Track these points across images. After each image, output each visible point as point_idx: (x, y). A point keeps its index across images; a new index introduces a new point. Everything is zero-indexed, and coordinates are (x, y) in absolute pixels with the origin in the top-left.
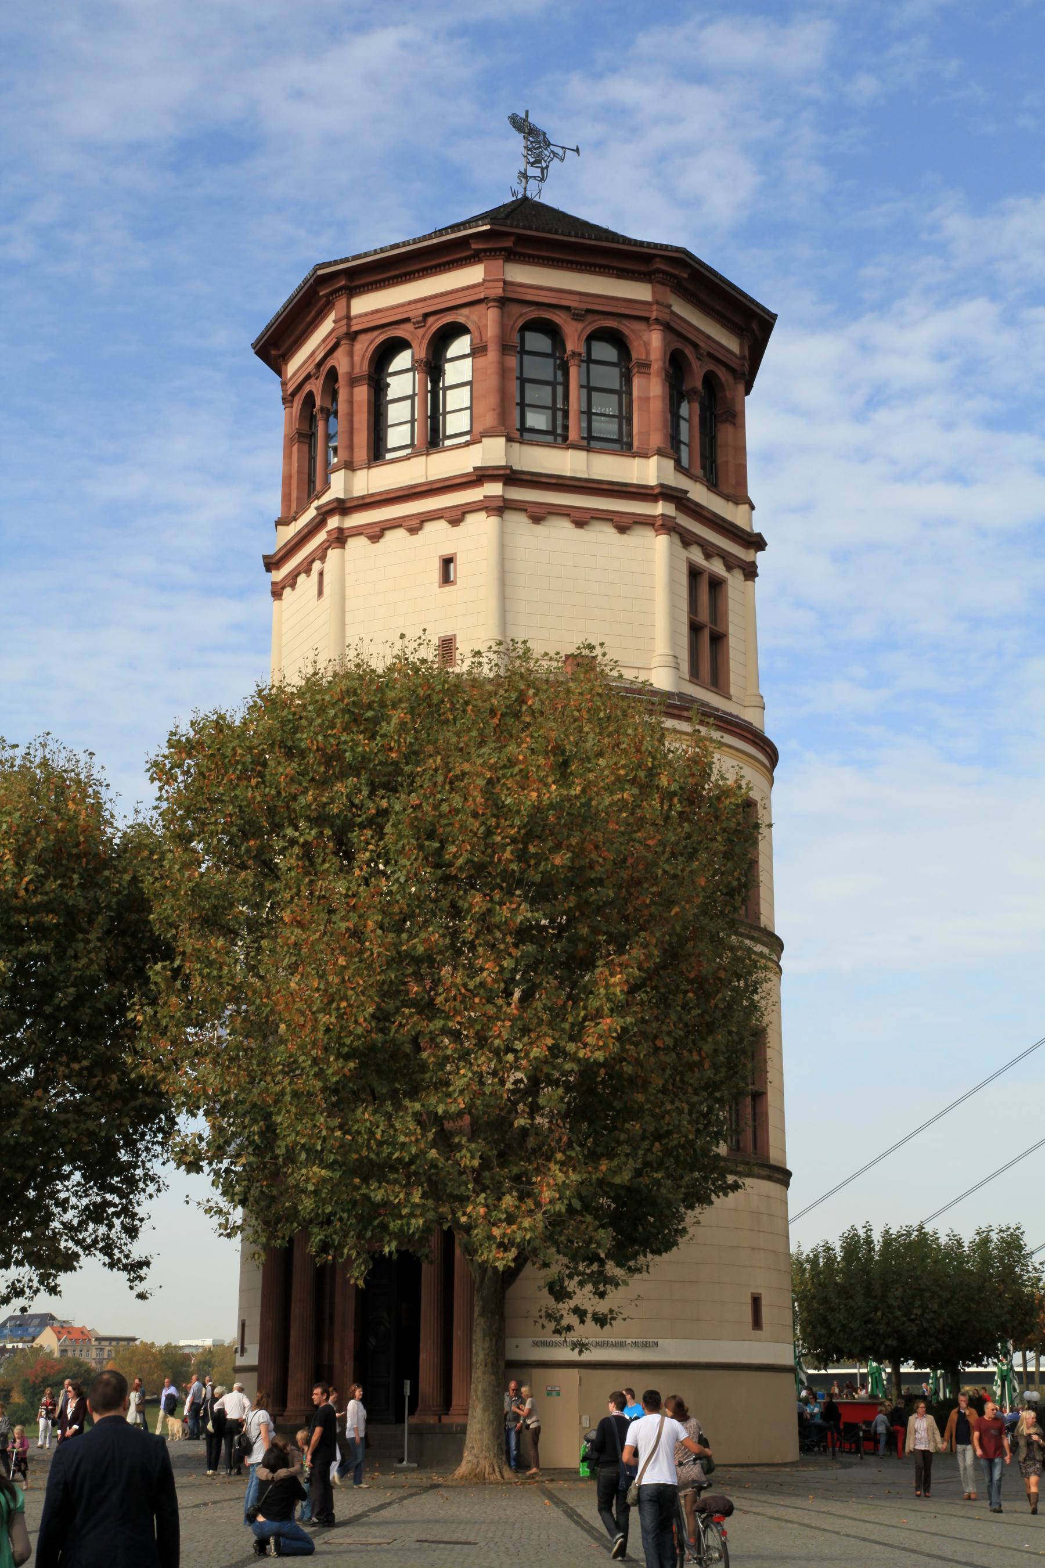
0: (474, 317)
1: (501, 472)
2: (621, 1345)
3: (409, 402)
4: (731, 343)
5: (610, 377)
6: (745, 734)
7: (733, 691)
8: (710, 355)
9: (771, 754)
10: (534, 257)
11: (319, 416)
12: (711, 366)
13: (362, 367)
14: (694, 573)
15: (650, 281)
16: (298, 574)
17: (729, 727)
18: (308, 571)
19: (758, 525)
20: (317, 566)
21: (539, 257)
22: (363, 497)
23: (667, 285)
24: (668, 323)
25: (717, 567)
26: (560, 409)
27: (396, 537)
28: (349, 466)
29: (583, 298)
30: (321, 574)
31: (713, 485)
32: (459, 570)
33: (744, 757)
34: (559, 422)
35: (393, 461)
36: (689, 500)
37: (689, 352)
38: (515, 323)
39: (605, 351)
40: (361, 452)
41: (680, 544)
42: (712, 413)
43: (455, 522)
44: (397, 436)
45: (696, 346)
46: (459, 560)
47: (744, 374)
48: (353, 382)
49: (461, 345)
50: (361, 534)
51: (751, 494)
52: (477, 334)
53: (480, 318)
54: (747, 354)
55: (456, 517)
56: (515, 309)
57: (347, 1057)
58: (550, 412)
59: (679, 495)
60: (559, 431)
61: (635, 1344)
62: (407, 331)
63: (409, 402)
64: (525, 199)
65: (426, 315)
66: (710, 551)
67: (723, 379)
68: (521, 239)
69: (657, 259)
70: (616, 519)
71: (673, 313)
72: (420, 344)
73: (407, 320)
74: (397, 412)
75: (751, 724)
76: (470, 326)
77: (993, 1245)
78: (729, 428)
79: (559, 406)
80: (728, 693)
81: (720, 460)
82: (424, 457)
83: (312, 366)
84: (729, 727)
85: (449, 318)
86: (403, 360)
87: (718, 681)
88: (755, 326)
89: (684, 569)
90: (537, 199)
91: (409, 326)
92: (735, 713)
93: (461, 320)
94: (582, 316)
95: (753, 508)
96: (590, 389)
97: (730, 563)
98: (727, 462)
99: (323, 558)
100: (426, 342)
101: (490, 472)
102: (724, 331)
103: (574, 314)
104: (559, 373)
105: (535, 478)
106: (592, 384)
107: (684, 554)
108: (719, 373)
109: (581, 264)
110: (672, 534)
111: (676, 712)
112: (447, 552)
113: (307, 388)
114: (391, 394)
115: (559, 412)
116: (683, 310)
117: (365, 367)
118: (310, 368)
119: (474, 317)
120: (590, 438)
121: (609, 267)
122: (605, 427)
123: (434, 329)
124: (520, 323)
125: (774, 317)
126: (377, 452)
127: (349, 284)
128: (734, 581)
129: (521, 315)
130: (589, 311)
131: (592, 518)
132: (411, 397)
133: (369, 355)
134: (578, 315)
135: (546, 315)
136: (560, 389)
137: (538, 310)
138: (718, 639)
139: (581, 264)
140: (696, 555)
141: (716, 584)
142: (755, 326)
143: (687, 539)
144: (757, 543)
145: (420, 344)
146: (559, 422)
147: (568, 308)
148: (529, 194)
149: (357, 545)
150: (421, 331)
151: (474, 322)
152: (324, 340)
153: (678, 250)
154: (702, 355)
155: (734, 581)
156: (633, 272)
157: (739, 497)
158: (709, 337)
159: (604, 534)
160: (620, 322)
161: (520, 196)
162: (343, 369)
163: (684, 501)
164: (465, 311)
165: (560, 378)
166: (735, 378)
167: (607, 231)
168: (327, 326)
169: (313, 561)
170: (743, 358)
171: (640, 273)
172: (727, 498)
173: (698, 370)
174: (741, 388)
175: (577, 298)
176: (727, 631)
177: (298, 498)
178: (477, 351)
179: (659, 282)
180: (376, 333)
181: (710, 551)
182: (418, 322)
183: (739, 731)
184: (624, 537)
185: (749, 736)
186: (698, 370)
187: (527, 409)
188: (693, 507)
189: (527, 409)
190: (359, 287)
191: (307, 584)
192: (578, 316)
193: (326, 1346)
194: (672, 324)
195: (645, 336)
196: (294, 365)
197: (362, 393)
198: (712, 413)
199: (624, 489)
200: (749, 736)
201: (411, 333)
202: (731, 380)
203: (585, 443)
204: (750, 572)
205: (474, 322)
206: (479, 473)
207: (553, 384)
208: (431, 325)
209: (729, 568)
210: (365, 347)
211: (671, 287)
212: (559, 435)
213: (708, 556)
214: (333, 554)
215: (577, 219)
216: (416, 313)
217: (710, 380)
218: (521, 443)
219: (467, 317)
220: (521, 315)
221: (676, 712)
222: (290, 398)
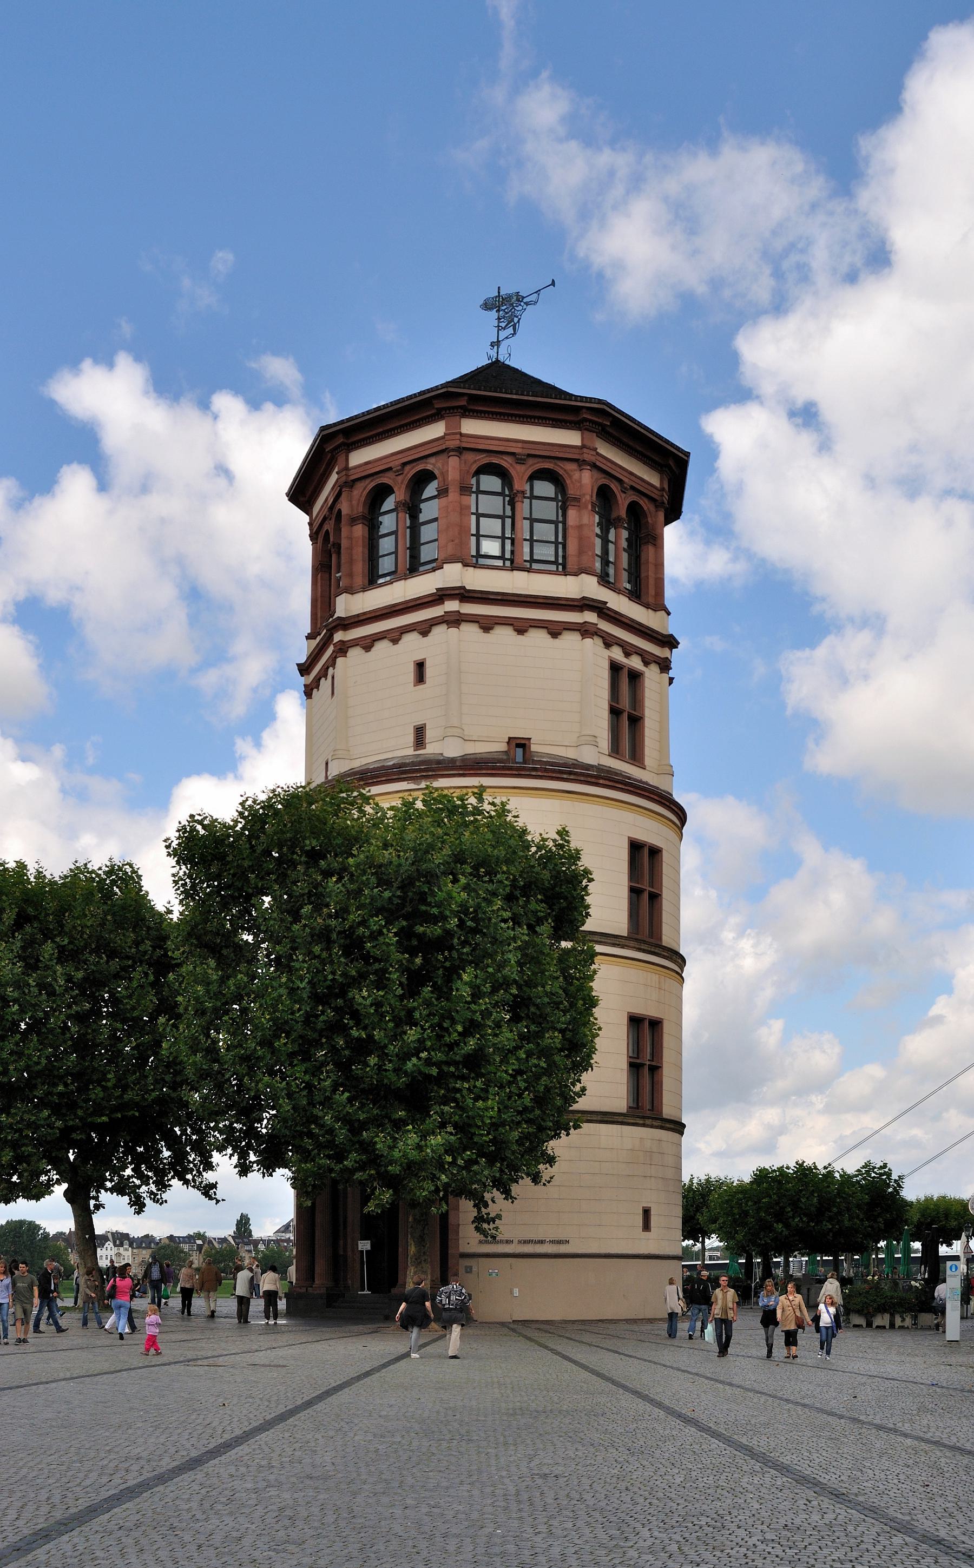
0: (439, 465)
1: (457, 592)
2: (542, 1242)
3: (535, 524)
4: (652, 478)
5: (548, 510)
6: (652, 796)
7: (648, 761)
8: (633, 488)
9: (681, 815)
10: (485, 412)
11: (333, 550)
12: (634, 497)
13: (360, 509)
14: (615, 668)
15: (579, 429)
16: (320, 679)
17: (639, 791)
18: (326, 676)
19: (672, 626)
20: (331, 670)
21: (512, 415)
22: (358, 615)
23: (594, 432)
24: (594, 464)
25: (635, 663)
26: (508, 538)
27: (382, 647)
28: (351, 591)
29: (526, 446)
30: (333, 677)
31: (636, 595)
32: (429, 672)
33: (652, 814)
34: (560, 553)
35: (381, 585)
36: (609, 609)
37: (614, 486)
38: (470, 468)
39: (544, 488)
40: (359, 580)
41: (602, 645)
42: (637, 536)
43: (368, 648)
44: (386, 564)
45: (620, 481)
46: (428, 665)
47: (663, 503)
48: (353, 521)
49: (431, 490)
50: (358, 645)
51: (668, 603)
52: (441, 479)
53: (443, 465)
54: (666, 487)
55: (424, 629)
56: (470, 457)
57: (40, 994)
58: (500, 540)
59: (600, 605)
60: (560, 561)
61: (552, 1242)
62: (390, 478)
63: (535, 524)
64: (497, 361)
65: (404, 464)
66: (629, 651)
67: (645, 508)
68: (473, 398)
69: (584, 410)
70: (550, 627)
71: (598, 454)
72: (400, 488)
73: (390, 469)
74: (386, 545)
75: (658, 788)
76: (436, 472)
77: (379, 1113)
78: (651, 549)
79: (508, 535)
80: (643, 764)
81: (643, 575)
82: (403, 581)
83: (326, 510)
84: (639, 791)
85: (420, 467)
86: (389, 504)
87: (636, 757)
88: (671, 463)
89: (606, 665)
90: (507, 362)
91: (390, 474)
92: (644, 779)
93: (429, 467)
94: (524, 460)
95: (669, 614)
96: (533, 521)
97: (647, 659)
98: (647, 577)
99: (334, 665)
100: (404, 486)
101: (449, 592)
102: (646, 468)
103: (518, 459)
104: (508, 508)
105: (484, 596)
106: (480, 512)
107: (606, 653)
108: (641, 502)
109: (523, 416)
110: (595, 637)
111: (593, 780)
112: (419, 657)
113: (326, 527)
114: (383, 531)
115: (509, 539)
116: (607, 451)
117: (361, 509)
118: (325, 511)
119: (439, 465)
120: (479, 555)
121: (546, 418)
122: (546, 552)
123: (410, 476)
124: (474, 468)
125: (688, 454)
126: (372, 580)
127: (345, 441)
128: (651, 675)
129: (475, 461)
130: (529, 455)
131: (531, 626)
132: (395, 533)
133: (363, 499)
134: (521, 459)
135: (495, 460)
136: (508, 521)
137: (490, 456)
138: (636, 721)
139: (523, 416)
140: (617, 654)
141: (635, 677)
142: (671, 463)
143: (609, 642)
144: (670, 642)
145: (400, 488)
146: (560, 553)
147: (513, 454)
148: (501, 358)
149: (355, 654)
150: (400, 478)
151: (439, 469)
152: (333, 488)
153: (600, 401)
154: (626, 488)
155: (651, 675)
156: (566, 421)
157: (658, 606)
158: (631, 473)
159: (538, 637)
160: (556, 464)
161: (494, 360)
162: (345, 510)
163: (605, 610)
164: (432, 460)
165: (509, 513)
166: (656, 507)
167: (553, 388)
168: (334, 478)
169: (328, 668)
170: (663, 489)
171: (571, 422)
172: (647, 606)
173: (623, 501)
174: (661, 516)
175: (520, 445)
176: (643, 714)
177: (321, 617)
178: (442, 492)
179: (586, 429)
180: (368, 481)
181: (629, 651)
182: (398, 471)
183: (647, 794)
184: (520, 637)
185: (656, 797)
186: (623, 501)
187: (481, 538)
188: (613, 614)
189: (481, 538)
190: (354, 443)
191: (325, 684)
192: (520, 459)
193: (341, 1242)
194: (598, 463)
195: (576, 475)
196: (316, 509)
197: (359, 531)
198: (637, 536)
199: (556, 602)
200: (656, 797)
201: (394, 480)
202: (652, 508)
203: (528, 565)
204: (665, 666)
205: (439, 469)
206: (440, 593)
207: (502, 518)
208: (408, 473)
209: (646, 663)
210: (361, 492)
211: (596, 433)
212: (508, 559)
213: (627, 655)
214: (340, 661)
215: (532, 377)
216: (396, 464)
217: (634, 510)
218: (475, 567)
219: (434, 465)
220: (475, 461)
221: (593, 780)
222: (315, 536)
